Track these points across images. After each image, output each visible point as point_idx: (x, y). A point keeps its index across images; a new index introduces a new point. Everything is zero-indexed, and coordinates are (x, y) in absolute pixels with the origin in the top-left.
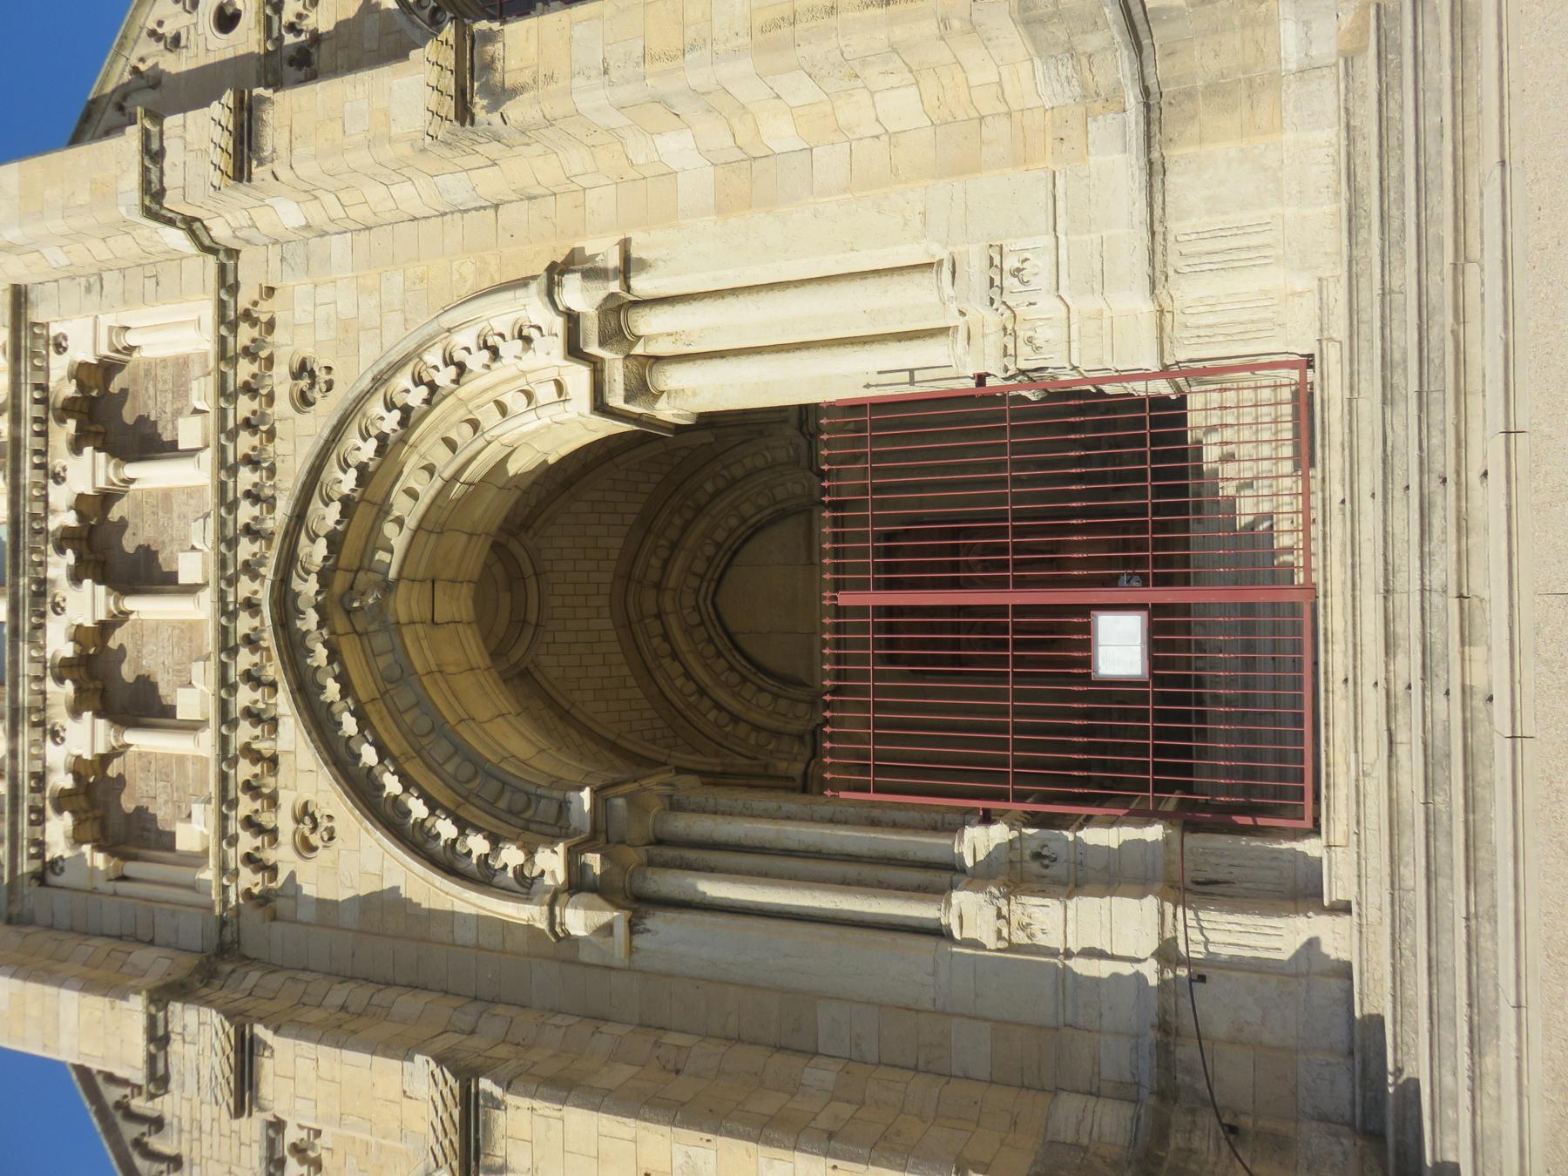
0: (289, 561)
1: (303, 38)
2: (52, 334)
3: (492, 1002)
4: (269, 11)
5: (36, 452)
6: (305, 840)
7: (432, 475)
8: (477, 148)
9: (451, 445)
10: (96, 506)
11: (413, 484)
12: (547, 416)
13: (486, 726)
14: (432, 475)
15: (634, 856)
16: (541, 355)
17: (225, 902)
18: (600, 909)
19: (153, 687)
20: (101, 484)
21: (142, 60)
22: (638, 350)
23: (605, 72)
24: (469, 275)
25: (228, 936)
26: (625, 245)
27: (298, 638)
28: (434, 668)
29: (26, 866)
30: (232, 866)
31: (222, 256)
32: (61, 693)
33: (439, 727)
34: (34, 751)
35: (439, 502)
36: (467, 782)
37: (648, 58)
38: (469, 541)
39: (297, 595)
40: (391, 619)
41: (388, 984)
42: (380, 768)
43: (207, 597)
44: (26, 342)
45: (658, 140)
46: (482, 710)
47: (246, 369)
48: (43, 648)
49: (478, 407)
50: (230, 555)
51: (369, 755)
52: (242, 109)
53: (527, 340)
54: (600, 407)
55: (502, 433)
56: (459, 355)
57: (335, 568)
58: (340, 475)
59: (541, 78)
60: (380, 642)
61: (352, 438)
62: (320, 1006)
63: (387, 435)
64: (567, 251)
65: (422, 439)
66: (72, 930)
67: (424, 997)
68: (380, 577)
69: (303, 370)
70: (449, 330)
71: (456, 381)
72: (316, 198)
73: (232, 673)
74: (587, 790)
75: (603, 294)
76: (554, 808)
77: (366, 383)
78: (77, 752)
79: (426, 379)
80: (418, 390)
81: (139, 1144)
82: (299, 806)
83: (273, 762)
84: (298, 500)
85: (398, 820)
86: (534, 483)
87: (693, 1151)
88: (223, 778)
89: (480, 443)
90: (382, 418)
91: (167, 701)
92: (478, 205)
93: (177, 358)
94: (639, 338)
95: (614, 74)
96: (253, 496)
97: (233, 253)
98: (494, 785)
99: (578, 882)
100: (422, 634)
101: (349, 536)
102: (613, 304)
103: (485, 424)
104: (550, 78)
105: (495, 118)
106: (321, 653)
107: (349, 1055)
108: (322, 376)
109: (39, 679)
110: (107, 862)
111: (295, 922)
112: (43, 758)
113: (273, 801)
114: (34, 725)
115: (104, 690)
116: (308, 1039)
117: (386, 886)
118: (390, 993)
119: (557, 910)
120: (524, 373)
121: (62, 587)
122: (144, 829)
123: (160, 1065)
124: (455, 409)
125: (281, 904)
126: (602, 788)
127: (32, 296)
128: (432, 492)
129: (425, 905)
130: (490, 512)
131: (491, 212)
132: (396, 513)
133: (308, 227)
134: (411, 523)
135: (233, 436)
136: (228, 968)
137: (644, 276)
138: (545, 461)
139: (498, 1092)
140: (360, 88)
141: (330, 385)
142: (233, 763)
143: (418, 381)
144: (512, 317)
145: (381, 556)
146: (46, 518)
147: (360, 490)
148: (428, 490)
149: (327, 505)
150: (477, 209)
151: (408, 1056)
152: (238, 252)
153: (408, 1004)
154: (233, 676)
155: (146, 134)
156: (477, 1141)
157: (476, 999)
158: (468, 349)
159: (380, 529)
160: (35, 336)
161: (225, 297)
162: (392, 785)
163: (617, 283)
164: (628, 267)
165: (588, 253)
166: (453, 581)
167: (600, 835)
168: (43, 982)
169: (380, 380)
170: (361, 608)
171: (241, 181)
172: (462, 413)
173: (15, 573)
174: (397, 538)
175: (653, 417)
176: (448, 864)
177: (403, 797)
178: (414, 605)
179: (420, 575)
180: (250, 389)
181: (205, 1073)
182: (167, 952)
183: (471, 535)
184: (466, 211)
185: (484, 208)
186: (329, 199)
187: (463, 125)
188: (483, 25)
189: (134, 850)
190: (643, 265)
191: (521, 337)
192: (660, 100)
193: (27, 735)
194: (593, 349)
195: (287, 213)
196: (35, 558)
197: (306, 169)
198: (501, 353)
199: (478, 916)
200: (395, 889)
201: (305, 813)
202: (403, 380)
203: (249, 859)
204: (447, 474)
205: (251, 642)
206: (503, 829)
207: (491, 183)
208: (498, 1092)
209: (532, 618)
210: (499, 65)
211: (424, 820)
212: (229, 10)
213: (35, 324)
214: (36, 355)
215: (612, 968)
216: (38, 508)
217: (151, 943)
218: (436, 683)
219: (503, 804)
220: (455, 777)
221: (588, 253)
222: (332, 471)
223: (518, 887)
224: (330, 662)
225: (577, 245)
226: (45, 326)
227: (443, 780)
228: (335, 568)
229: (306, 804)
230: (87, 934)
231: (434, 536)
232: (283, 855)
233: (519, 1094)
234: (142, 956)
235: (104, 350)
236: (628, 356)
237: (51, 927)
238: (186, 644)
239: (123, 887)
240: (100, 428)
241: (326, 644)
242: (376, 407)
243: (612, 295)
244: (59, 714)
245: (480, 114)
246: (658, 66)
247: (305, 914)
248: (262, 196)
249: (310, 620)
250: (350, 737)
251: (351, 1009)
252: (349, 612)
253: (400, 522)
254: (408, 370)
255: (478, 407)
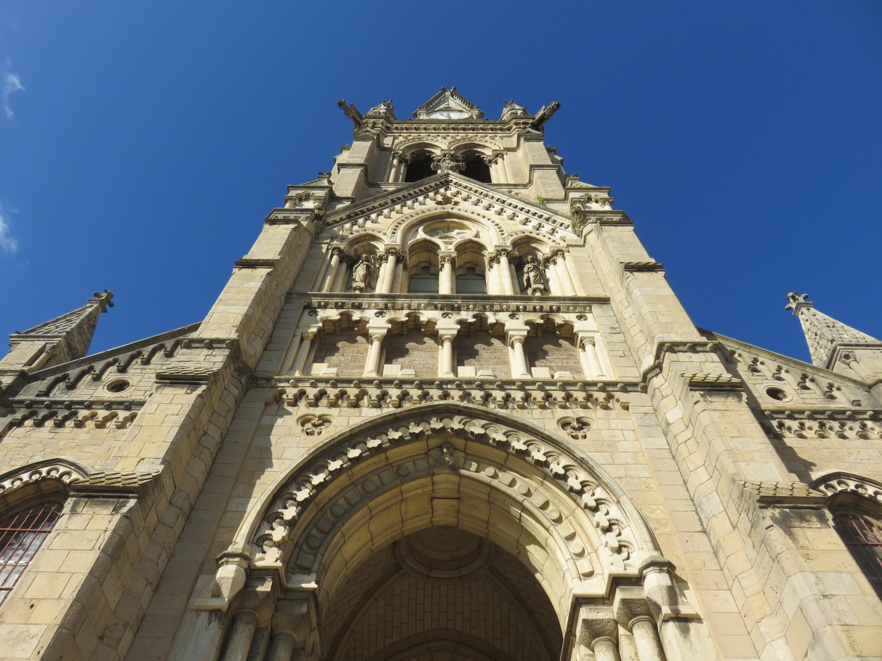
0: (471, 414)
1: (778, 430)
2: (587, 314)
3: (188, 518)
4: (787, 412)
5: (525, 307)
6: (309, 421)
7: (525, 495)
8: (743, 514)
9: (545, 506)
10: (500, 333)
11: (519, 484)
12: (568, 566)
13: (365, 528)
14: (525, 495)
15: (265, 617)
16: (610, 559)
17: (280, 381)
18: (232, 588)
19: (403, 356)
20: (510, 333)
21: (740, 355)
22: (622, 631)
23: (825, 596)
24: (657, 514)
25: (260, 382)
26: (696, 619)
27: (426, 419)
28: (405, 496)
29: (315, 301)
30: (300, 385)
31: (642, 384)
32: (402, 316)
33: (368, 496)
34: (373, 305)
35: (508, 500)
36: (331, 511)
37: (846, 628)
38: (483, 521)
39: (451, 419)
40: (435, 471)
41: (214, 461)
42: (346, 459)
43: (451, 376)
44: (581, 303)
45: (782, 642)
46: (376, 525)
47: (580, 396)
48: (425, 309)
49: (571, 523)
50: (474, 386)
51: (354, 453)
52: (731, 386)
53: (619, 550)
54: (579, 602)
55: (555, 539)
56: (603, 508)
57: (467, 439)
58: (522, 441)
59: (806, 552)
60: (422, 464)
61: (545, 448)
62: (210, 422)
63: (548, 466)
64: (684, 578)
65: (548, 489)
66: (279, 317)
67: (201, 478)
68: (461, 465)
69: (583, 424)
70: (618, 502)
71: (586, 506)
72: (687, 427)
73: (408, 386)
74: (316, 586)
75: (659, 601)
76: (306, 564)
77: (579, 454)
78: (371, 322)
79: (586, 489)
80: (580, 486)
81: (162, 347)
82: (329, 418)
83: (356, 405)
84: (507, 418)
85: (312, 468)
86: (522, 565)
87: (35, 641)
88: (349, 381)
89: (547, 524)
90: (558, 464)
91: (394, 361)
92: (703, 520)
93: (581, 368)
94: (631, 631)
95: (825, 602)
96: (507, 398)
97: (645, 390)
98: (326, 527)
99: (253, 575)
100: (426, 489)
101: (486, 448)
102: (653, 610)
103: (559, 527)
104: (807, 557)
105: (769, 522)
106: (417, 430)
107: (175, 430)
108: (580, 434)
109: (409, 307)
110: (312, 333)
111: (262, 415)
112: (369, 308)
113: (333, 405)
114: (386, 305)
115: (402, 335)
116: (191, 411)
117: (274, 461)
118: (208, 459)
119: (237, 559)
120: (596, 551)
121: (455, 317)
122: (327, 351)
123: (197, 345)
124: (568, 508)
125: (275, 407)
126: (316, 598)
127: (605, 306)
128: (514, 495)
129: (258, 482)
130: (503, 534)
131: (700, 528)
132: (500, 474)
133: (668, 424)
134: (494, 483)
135: (541, 388)
136: (243, 380)
137: (677, 632)
138: (537, 571)
139: (125, 510)
140: (763, 446)
141: (575, 437)
142: (357, 386)
143: (584, 484)
144: (632, 540)
145: (474, 466)
146: (491, 311)
147: (514, 452)
148: (516, 492)
149: (504, 434)
150: (700, 519)
151: (164, 461)
152: (646, 392)
153: (199, 469)
154: (405, 387)
155: (704, 345)
156: (98, 497)
157: (192, 509)
158: (607, 513)
159: (490, 465)
160: (585, 308)
161: (619, 385)
162: (334, 465)
163: (669, 612)
164: (683, 620)
165: (686, 592)
166: (458, 512)
167: (284, 593)
168: (254, 300)
169: (582, 463)
170: (443, 453)
171: (690, 385)
172: (565, 512)
173: (463, 298)
174: (486, 474)
175: (573, 646)
176: (281, 495)
177: (327, 472)
178: (444, 485)
179: (462, 489)
180: (568, 397)
181: (187, 364)
182: (259, 354)
183: (488, 523)
184: (697, 513)
185: (702, 524)
186: (688, 434)
187: (758, 501)
188: (829, 515)
189: (316, 346)
190: (685, 632)
191: (621, 547)
192: (816, 638)
193: (381, 302)
194: (619, 595)
195: (674, 413)
196: (471, 306)
197: (705, 418)
198: (608, 534)
199: (245, 512)
200: (271, 466)
201: (324, 420)
202: (583, 476)
203: (302, 393)
204: (526, 503)
205: (425, 396)
206: (298, 530)
207: (720, 526)
208: (125, 510)
209: (434, 574)
210: (804, 524)
211: (310, 482)
212: (780, 396)
213: (591, 307)
214: (575, 308)
215: (189, 597)
216: (496, 307)
217: (265, 349)
218: (395, 496)
219: (314, 532)
220: (335, 504)
221: (686, 592)
222: (524, 437)
223: (258, 536)
224: (411, 434)
225: (690, 585)
226: (590, 312)
227: (334, 496)
228: (467, 439)
229: (330, 422)
230: (276, 324)
231: (486, 497)
232: (302, 409)
233: (119, 523)
234: (259, 344)
235: (580, 335)
236: (616, 622)
237: (282, 310)
238: (426, 370)
239: (298, 339)
240: (540, 335)
241: (422, 432)
242: (565, 461)
243: (659, 608)
244: (390, 315)
245: (768, 512)
246: (843, 636)
247: (266, 420)
248: (682, 399)
249: (436, 424)
250: (366, 444)
251: (204, 438)
252: (440, 447)
253: (495, 476)
254: (590, 479)
255: (571, 523)
